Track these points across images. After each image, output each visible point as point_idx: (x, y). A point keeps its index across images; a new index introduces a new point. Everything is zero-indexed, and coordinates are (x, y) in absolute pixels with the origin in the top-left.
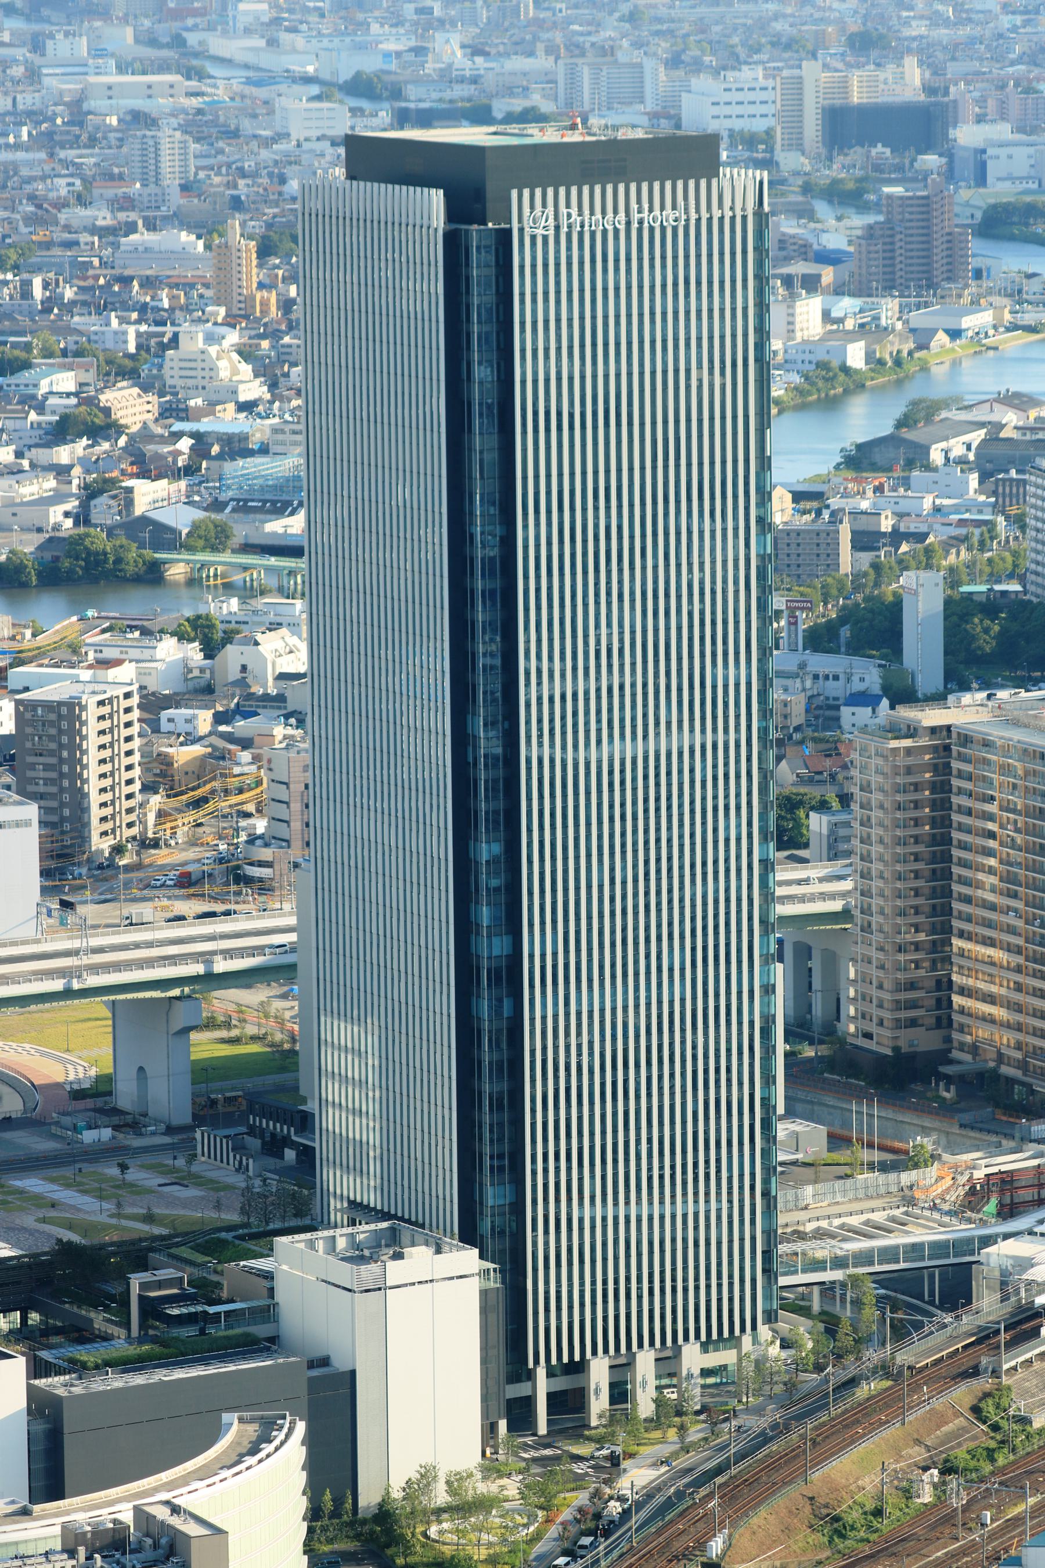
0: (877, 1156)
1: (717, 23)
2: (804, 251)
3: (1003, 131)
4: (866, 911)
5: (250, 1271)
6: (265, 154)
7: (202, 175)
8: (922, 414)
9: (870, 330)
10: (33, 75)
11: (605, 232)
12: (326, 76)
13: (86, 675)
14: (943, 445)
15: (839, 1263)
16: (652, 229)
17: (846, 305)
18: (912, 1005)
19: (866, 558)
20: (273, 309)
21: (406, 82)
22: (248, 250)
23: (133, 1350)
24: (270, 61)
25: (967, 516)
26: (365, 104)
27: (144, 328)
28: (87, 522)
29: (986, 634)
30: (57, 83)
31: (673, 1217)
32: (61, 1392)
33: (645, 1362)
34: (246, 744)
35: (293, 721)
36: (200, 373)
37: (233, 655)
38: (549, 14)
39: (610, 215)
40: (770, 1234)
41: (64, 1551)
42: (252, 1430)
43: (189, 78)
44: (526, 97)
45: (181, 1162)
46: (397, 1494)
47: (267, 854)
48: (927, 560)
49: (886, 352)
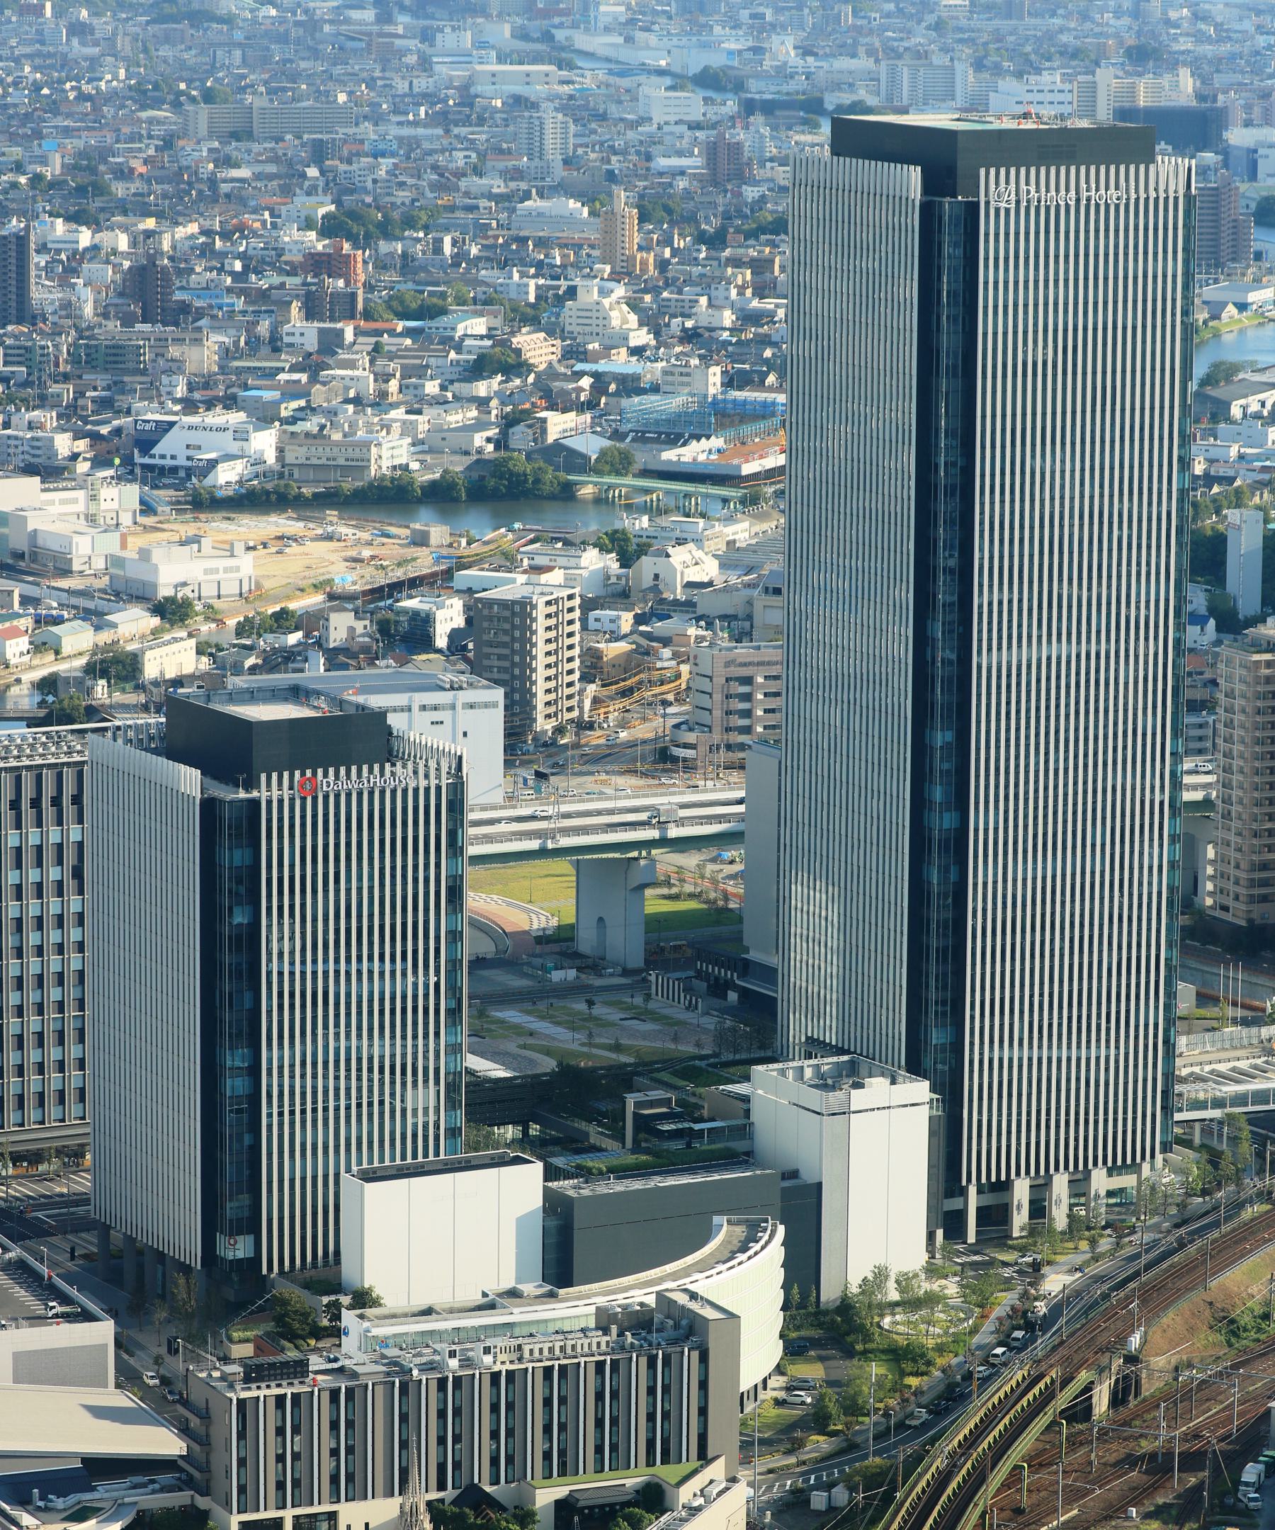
0: (1239, 1013)
1: (1011, 34)
4: (1227, 800)
5: (729, 1094)
6: (631, 135)
7: (580, 151)
8: (1222, 375)
10: (425, 64)
11: (1058, 206)
12: (676, 69)
13: (522, 578)
14: (1243, 402)
15: (1218, 1103)
16: (1097, 205)
20: (651, 268)
21: (748, 77)
22: (631, 217)
23: (631, 1159)
24: (626, 55)
25: (1268, 463)
27: (541, 281)
28: (507, 448)
31: (1079, 1059)
32: (571, 1193)
33: (1060, 1183)
34: (666, 642)
35: (702, 623)
36: (594, 322)
37: (647, 565)
38: (865, 22)
39: (1063, 192)
40: (1170, 1077)
41: (597, 1328)
42: (740, 1231)
43: (560, 69)
44: (852, 92)
45: (638, 1000)
46: (854, 1289)
47: (691, 738)
48: (1238, 500)
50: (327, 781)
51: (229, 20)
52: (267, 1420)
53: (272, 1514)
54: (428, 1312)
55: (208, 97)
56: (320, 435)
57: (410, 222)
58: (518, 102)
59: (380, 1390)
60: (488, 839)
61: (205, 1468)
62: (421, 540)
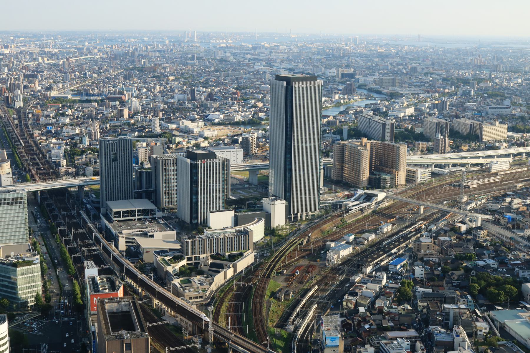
2: (337, 89)
3: (362, 76)
9: (344, 99)
10: (253, 67)
17: (341, 95)
30: (256, 68)
33: (305, 214)
48: (347, 124)
50: (206, 161)
51: (229, 61)
52: (190, 244)
55: (224, 71)
57: (247, 88)
58: (265, 72)
61: (183, 250)
62: (240, 129)
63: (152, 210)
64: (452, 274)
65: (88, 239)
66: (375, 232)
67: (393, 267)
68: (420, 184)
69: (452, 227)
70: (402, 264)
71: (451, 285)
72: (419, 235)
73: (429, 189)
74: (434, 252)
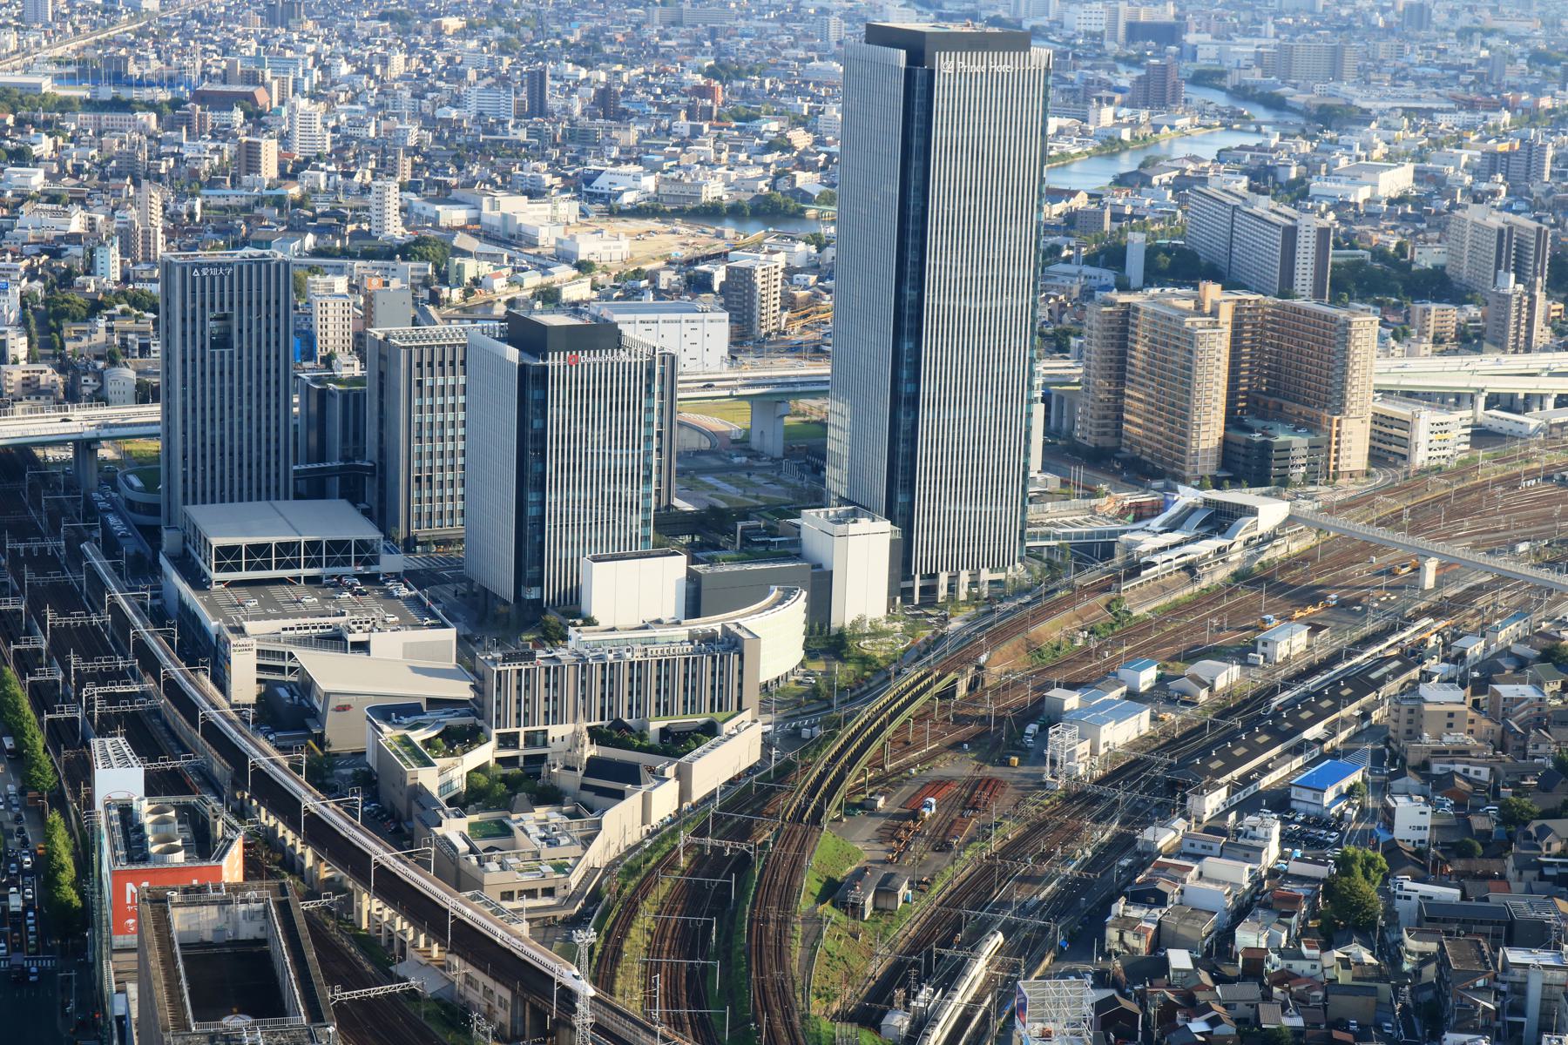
2: (1109, 87)
3: (1208, 37)
13: (763, 257)
17: (1125, 111)
18: (1104, 426)
19: (1116, 225)
26: (925, 10)
29: (1164, 261)
33: (965, 577)
40: (1023, 522)
46: (847, 624)
47: (830, 341)
48: (1143, 228)
49: (1140, 133)
50: (584, 358)
53: (514, 730)
54: (613, 629)
56: (678, 181)
59: (572, 669)
60: (688, 390)
61: (481, 706)
62: (720, 235)
63: (363, 545)
64: (1543, 832)
65: (109, 652)
66: (1241, 654)
67: (1308, 795)
68: (1424, 472)
69: (1546, 643)
70: (1345, 784)
71: (1535, 873)
72: (1415, 673)
73: (1461, 493)
74: (1471, 741)
